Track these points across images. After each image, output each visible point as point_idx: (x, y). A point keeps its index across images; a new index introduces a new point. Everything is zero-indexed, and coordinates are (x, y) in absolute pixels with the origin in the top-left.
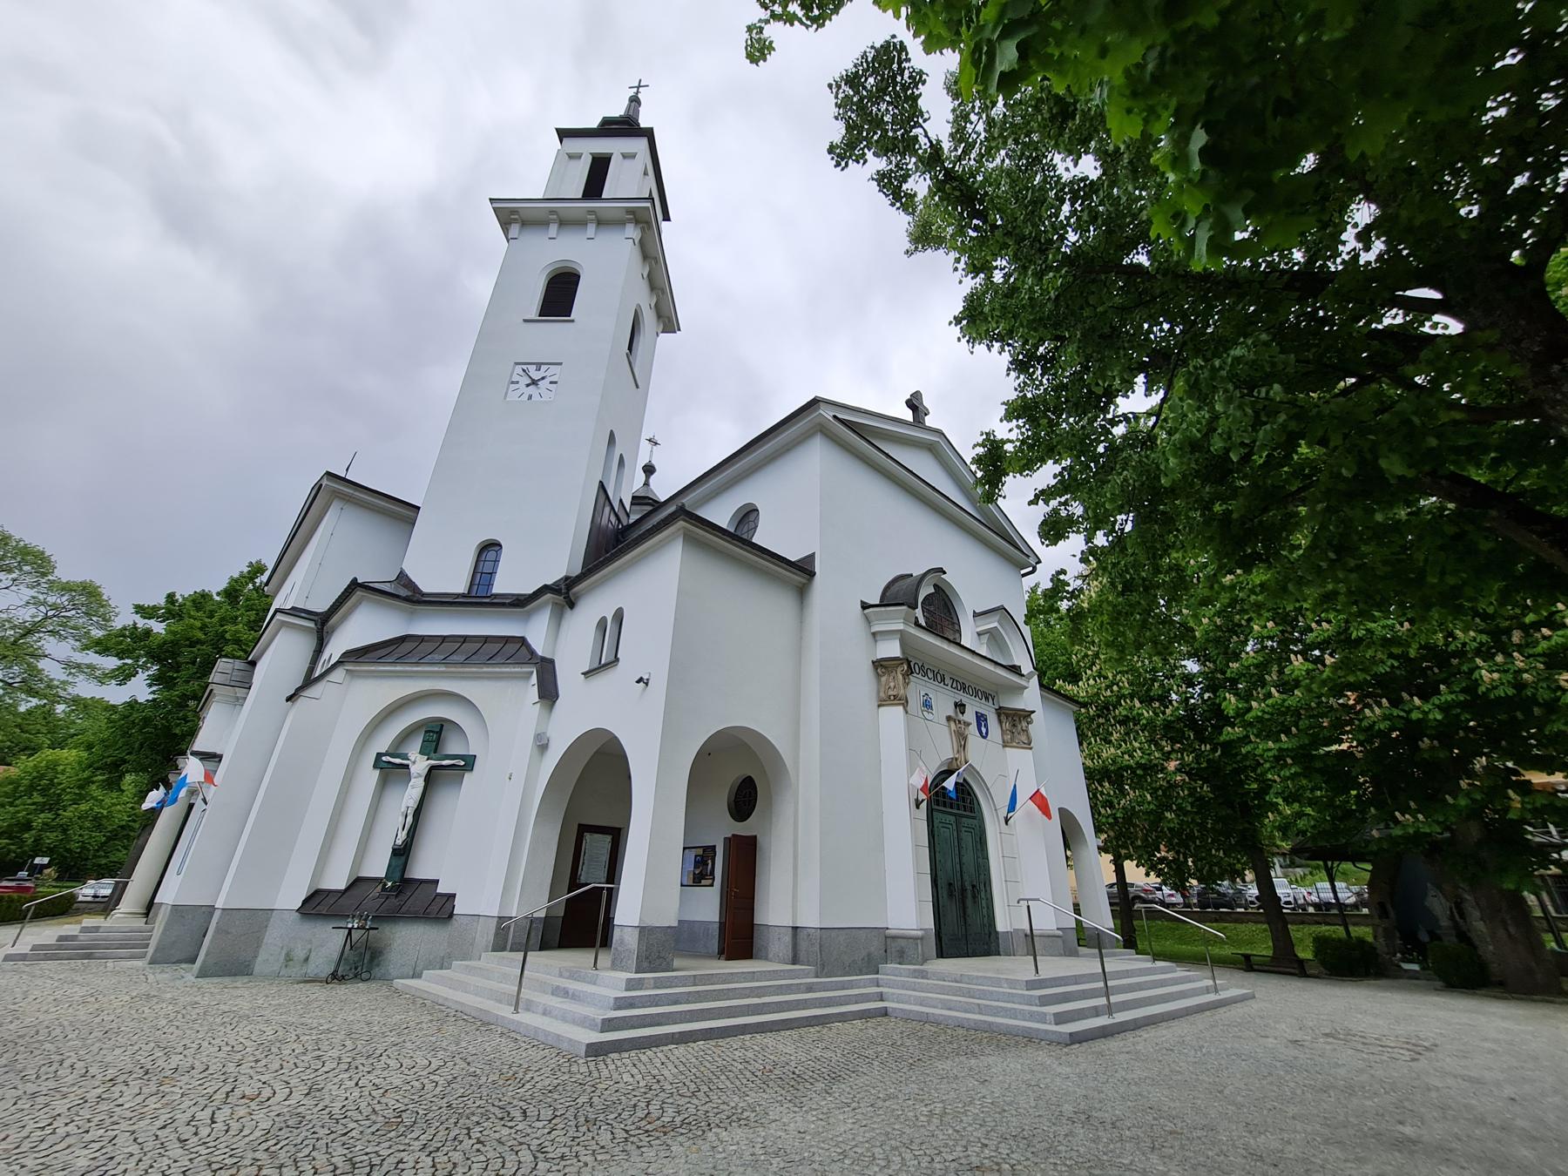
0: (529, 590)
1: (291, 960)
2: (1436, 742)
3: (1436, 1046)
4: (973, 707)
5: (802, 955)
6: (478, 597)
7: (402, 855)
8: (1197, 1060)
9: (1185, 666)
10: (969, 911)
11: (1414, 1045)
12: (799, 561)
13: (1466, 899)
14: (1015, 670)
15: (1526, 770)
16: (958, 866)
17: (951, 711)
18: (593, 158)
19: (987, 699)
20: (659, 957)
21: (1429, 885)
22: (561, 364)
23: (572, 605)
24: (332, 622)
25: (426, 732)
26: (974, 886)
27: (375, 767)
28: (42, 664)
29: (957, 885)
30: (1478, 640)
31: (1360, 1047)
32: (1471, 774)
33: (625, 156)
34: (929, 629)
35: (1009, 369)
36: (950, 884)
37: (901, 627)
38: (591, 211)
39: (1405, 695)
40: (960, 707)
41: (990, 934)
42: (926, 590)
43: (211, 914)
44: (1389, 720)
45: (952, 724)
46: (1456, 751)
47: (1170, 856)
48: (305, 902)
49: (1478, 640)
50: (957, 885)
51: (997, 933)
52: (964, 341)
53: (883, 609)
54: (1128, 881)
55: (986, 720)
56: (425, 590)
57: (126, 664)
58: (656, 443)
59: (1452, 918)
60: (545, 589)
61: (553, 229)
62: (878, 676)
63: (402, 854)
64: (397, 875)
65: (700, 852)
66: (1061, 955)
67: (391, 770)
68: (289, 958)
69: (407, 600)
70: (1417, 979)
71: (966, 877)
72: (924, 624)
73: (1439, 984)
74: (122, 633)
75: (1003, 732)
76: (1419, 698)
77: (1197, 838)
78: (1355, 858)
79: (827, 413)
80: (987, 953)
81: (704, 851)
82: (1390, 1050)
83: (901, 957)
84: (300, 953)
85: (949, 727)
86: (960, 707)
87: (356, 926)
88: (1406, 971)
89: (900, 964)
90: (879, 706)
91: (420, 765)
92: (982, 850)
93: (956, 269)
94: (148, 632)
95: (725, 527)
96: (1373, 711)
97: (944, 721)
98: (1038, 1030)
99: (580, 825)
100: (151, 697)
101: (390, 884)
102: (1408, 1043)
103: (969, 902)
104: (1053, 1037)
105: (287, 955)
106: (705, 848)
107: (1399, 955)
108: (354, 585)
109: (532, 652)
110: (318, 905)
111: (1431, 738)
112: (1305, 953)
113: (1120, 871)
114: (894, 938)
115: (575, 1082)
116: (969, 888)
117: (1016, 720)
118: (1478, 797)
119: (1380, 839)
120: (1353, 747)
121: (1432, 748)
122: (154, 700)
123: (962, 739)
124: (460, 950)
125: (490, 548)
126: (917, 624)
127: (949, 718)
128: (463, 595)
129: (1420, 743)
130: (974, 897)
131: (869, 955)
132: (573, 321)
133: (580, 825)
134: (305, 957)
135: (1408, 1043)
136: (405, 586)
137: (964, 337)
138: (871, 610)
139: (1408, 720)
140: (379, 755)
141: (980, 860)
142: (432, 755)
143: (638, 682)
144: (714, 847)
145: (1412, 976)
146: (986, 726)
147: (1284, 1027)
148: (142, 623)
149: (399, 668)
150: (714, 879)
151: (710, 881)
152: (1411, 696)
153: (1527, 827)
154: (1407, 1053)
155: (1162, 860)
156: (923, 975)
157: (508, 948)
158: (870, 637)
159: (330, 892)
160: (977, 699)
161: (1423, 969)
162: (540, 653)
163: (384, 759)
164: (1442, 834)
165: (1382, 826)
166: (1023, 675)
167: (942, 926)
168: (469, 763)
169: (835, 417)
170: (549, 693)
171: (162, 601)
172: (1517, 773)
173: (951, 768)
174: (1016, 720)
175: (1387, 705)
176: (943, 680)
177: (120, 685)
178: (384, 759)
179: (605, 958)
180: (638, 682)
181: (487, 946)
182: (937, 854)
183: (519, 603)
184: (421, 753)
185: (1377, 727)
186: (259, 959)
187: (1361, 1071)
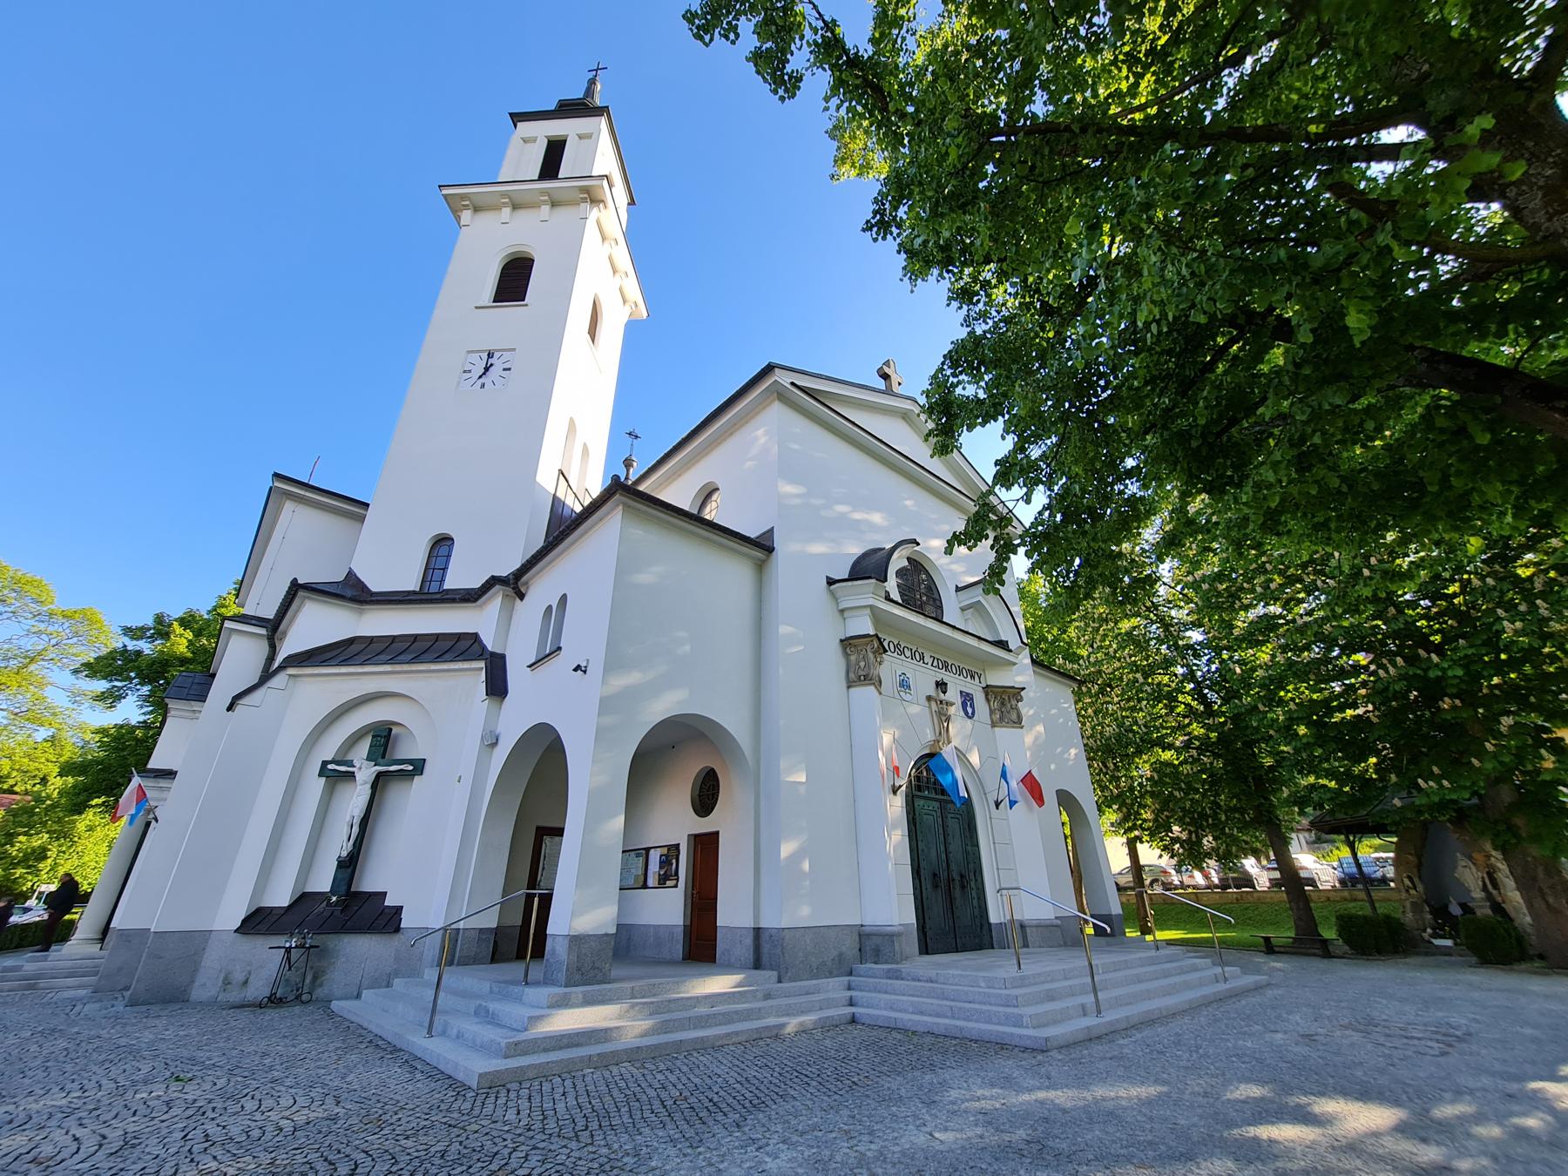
0: (477, 585)
1: (229, 983)
2: (1458, 702)
3: (1470, 1034)
4: (956, 685)
5: (765, 959)
6: (430, 594)
7: (348, 867)
8: (1189, 1064)
9: (1190, 637)
10: (958, 901)
11: (1444, 1035)
12: (758, 537)
13: (1500, 869)
14: (1002, 645)
15: (1559, 728)
16: (944, 856)
17: (932, 691)
18: (549, 141)
19: (972, 677)
20: (593, 968)
21: (1458, 854)
22: (514, 350)
23: (521, 596)
24: (282, 627)
25: (373, 737)
26: (962, 876)
27: (320, 775)
28: (50, 692)
29: (943, 875)
30: (1498, 588)
31: (1382, 1040)
32: (1498, 735)
33: (580, 137)
34: (907, 603)
35: (950, 299)
36: (935, 875)
37: (871, 602)
38: (543, 192)
39: (1422, 652)
40: (942, 686)
41: (982, 925)
42: (898, 562)
43: (458, 933)
44: (1405, 679)
45: (933, 704)
46: (1481, 711)
47: (1184, 836)
48: (244, 921)
49: (1498, 588)
50: (943, 875)
51: (990, 924)
52: (906, 279)
53: (850, 583)
54: (1142, 863)
55: (972, 699)
56: (374, 589)
57: (115, 686)
58: (637, 437)
59: (1485, 889)
60: (494, 581)
61: (507, 211)
62: (846, 655)
63: (349, 865)
64: (343, 889)
65: (665, 851)
66: (1061, 946)
67: (336, 775)
68: (227, 982)
69: (354, 600)
70: (1451, 955)
71: (953, 866)
72: (900, 601)
73: (1474, 959)
74: (112, 655)
75: (992, 712)
76: (1437, 655)
77: (1209, 816)
78: (1378, 830)
79: (784, 378)
80: (979, 947)
81: (669, 850)
82: (1416, 1042)
83: (877, 955)
84: (239, 976)
85: (930, 707)
86: (942, 686)
87: (294, 945)
88: (1437, 947)
89: (876, 963)
90: (849, 687)
91: (366, 772)
92: (971, 837)
93: (826, 109)
94: (139, 653)
95: (686, 508)
96: (1387, 671)
97: (923, 701)
98: (1012, 1035)
99: (538, 828)
100: (142, 718)
101: (334, 899)
102: (1437, 1033)
103: (957, 893)
104: (1028, 1043)
105: (226, 978)
106: (669, 847)
107: (1429, 930)
108: (295, 588)
109: (484, 648)
110: (258, 922)
111: (1452, 697)
112: (1329, 933)
113: (1133, 854)
114: (869, 935)
115: (445, 1124)
116: (957, 878)
117: (1005, 703)
118: (1507, 759)
119: (1402, 807)
120: (1369, 712)
121: (1454, 708)
122: (145, 722)
123: (943, 717)
124: (407, 968)
125: (442, 545)
126: (888, 598)
127: (929, 698)
128: (414, 592)
129: (1440, 703)
130: (963, 887)
131: (841, 955)
132: (526, 305)
133: (538, 828)
134: (244, 979)
135: (1437, 1033)
136: (353, 586)
137: (905, 276)
138: (837, 585)
139: (1425, 679)
140: (325, 763)
141: (969, 848)
142: (380, 760)
143: (575, 670)
144: (677, 846)
145: (1445, 952)
146: (972, 706)
147: (1298, 1018)
148: (132, 645)
149: (344, 670)
150: (678, 880)
151: (674, 882)
152: (1429, 653)
153: (1561, 788)
154: (1435, 1045)
155: (1175, 840)
156: (897, 975)
157: (456, 961)
158: (837, 614)
159: (272, 909)
160: (961, 677)
161: (1456, 944)
162: (490, 649)
163: (330, 767)
164: (1469, 800)
165: (1404, 794)
166: (1011, 651)
167: (927, 920)
168: (419, 766)
169: (792, 384)
170: (497, 686)
171: (150, 622)
172: (1548, 731)
173: (933, 751)
174: (1005, 703)
175: (1402, 663)
176: (922, 658)
177: (111, 707)
178: (330, 767)
179: (536, 970)
180: (575, 670)
181: (433, 961)
182: (919, 843)
183: (470, 597)
184: (368, 759)
185: (1391, 688)
186: (197, 984)
187: (1382, 1071)
